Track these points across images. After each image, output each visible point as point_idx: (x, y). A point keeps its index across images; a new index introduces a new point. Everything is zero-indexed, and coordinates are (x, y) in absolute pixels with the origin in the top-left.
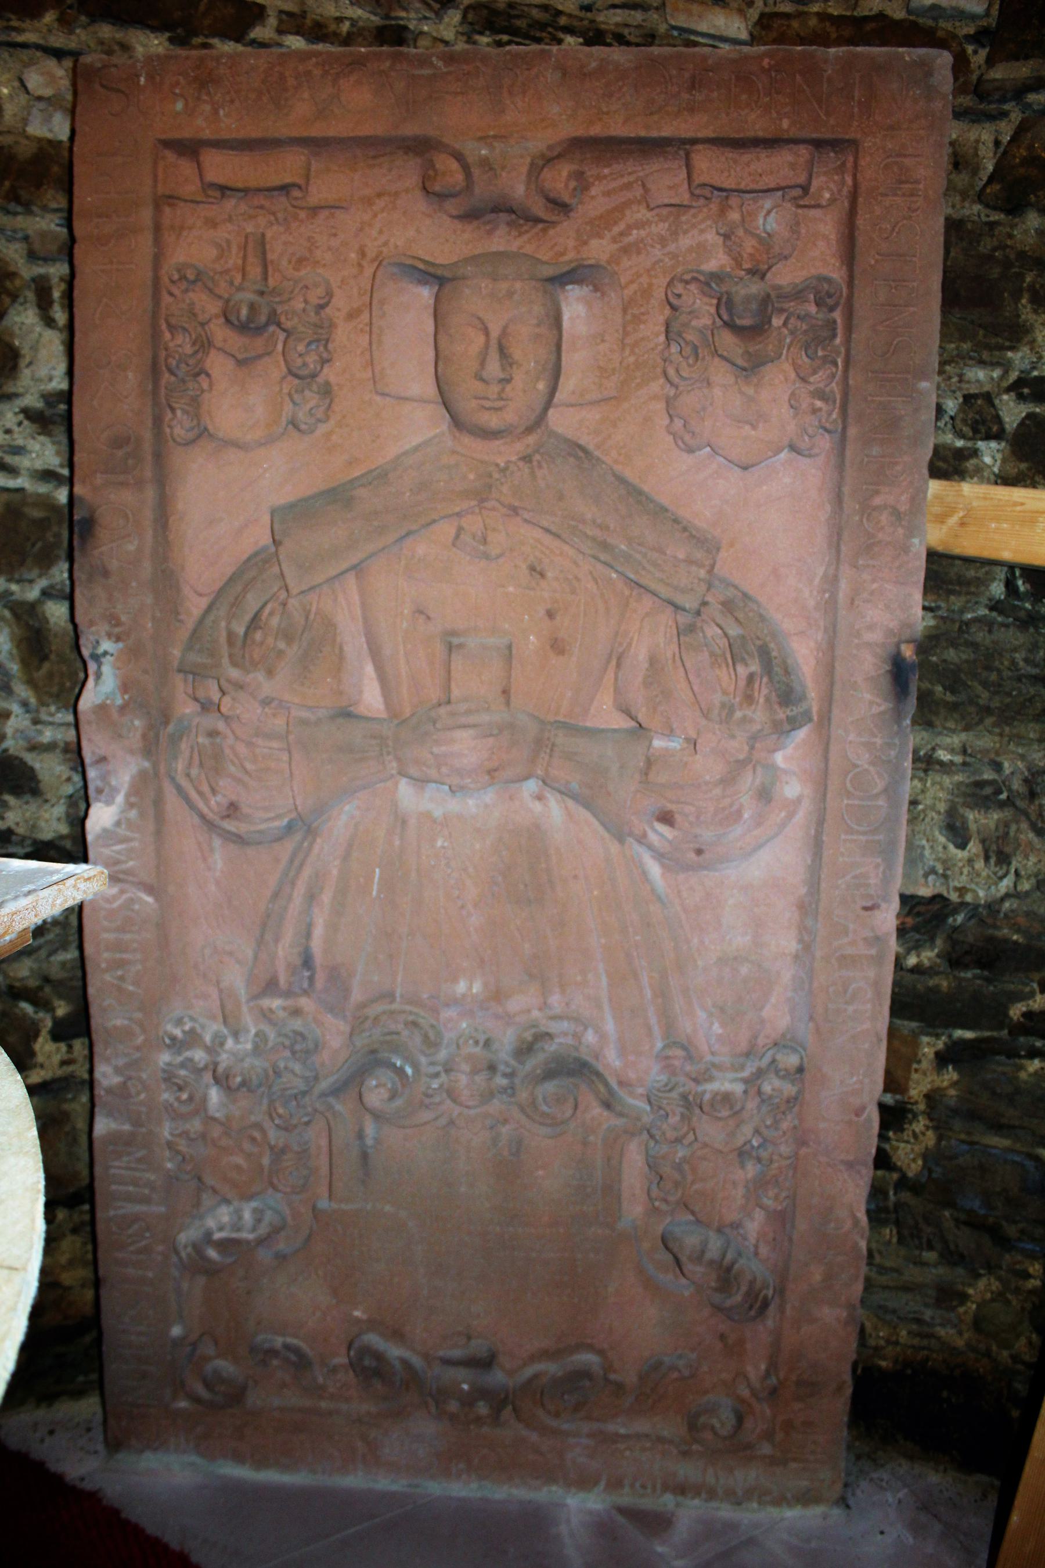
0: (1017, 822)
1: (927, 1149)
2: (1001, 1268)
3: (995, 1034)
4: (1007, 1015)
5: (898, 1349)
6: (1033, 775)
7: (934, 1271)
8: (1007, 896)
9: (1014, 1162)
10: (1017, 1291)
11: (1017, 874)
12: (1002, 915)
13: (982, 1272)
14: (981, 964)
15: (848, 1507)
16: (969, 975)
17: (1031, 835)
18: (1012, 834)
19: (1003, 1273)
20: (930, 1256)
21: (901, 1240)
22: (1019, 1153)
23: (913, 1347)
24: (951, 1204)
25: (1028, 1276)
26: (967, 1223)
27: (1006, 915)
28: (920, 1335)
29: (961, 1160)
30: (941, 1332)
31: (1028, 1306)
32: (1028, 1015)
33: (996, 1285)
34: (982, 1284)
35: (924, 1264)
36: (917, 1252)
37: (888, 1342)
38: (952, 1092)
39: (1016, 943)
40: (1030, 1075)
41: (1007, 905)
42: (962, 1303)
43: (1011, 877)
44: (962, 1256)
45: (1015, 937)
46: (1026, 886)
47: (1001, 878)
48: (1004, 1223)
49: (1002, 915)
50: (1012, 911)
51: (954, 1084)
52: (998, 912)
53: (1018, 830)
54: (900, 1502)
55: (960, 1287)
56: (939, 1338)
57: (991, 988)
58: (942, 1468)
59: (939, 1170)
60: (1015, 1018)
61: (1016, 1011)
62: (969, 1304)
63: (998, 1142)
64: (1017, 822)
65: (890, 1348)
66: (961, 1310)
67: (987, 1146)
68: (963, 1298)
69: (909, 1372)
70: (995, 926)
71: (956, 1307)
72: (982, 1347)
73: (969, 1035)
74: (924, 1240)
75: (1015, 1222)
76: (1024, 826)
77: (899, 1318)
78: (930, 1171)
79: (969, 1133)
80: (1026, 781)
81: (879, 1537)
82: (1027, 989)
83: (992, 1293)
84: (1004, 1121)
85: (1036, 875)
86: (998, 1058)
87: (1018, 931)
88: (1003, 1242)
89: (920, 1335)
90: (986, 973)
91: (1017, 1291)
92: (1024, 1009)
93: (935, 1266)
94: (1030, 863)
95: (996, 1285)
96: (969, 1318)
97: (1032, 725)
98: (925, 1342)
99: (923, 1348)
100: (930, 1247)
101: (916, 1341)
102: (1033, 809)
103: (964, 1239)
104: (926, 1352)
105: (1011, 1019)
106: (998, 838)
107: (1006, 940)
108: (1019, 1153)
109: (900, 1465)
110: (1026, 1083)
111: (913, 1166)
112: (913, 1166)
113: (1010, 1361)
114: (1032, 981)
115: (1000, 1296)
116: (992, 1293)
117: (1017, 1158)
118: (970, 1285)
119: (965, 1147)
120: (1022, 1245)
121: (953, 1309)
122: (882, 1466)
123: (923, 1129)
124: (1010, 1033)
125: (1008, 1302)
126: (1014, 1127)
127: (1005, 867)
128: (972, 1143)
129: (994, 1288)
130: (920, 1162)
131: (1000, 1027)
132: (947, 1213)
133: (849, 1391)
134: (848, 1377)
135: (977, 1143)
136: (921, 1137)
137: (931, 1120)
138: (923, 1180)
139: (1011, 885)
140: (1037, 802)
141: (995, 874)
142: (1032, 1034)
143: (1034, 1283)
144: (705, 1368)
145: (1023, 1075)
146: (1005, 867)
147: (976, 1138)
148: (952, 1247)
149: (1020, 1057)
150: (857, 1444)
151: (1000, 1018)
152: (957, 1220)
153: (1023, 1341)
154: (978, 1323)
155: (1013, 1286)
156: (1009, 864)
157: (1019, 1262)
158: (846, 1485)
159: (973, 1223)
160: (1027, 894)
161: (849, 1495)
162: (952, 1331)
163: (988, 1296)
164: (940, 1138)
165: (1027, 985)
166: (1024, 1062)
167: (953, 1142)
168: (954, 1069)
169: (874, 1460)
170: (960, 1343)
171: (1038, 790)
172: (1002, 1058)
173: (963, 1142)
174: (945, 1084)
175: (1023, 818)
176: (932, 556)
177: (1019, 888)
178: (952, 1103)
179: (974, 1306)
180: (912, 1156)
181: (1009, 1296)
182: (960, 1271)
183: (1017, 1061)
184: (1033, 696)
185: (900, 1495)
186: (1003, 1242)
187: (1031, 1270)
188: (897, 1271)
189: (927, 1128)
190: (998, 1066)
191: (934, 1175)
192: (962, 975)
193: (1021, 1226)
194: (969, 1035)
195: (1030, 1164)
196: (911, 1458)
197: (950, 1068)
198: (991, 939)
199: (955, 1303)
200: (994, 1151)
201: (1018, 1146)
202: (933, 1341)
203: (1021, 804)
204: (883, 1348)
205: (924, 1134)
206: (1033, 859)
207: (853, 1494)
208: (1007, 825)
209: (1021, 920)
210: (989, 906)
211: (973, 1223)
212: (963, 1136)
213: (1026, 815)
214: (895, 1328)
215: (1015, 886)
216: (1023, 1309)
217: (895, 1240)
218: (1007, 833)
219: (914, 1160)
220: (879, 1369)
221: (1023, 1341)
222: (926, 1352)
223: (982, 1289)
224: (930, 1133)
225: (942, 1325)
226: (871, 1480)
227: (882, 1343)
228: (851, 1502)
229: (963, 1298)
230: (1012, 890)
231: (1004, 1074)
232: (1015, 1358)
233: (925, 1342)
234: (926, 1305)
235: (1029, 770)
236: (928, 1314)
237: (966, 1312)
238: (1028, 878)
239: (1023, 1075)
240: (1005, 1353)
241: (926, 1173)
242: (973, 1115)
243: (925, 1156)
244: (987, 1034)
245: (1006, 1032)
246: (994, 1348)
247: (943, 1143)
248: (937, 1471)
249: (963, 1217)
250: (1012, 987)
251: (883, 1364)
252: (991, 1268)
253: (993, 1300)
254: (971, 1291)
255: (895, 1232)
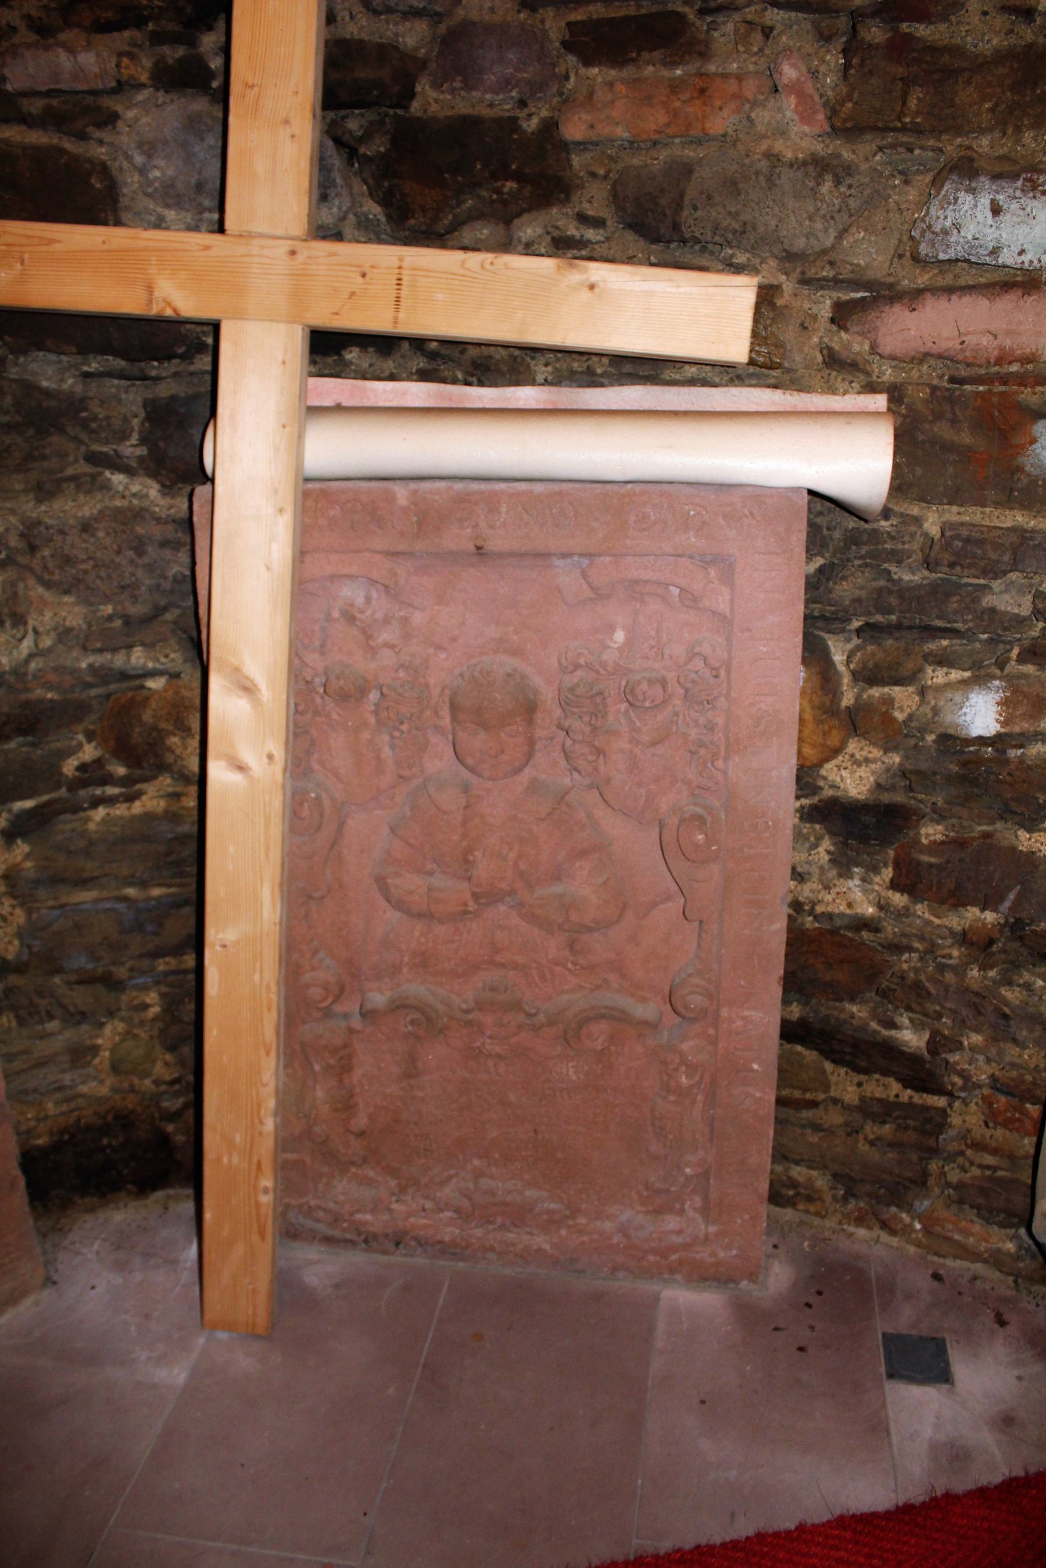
0: (24, 580)
1: (19, 927)
2: (120, 1009)
3: (53, 795)
4: (61, 774)
5: (50, 1122)
6: (28, 528)
7: (61, 1038)
8: (31, 656)
9: (108, 909)
10: (142, 1023)
11: (36, 631)
12: (30, 677)
13: (104, 1020)
14: (22, 731)
15: (55, 1283)
16: (12, 745)
17: (40, 590)
18: (21, 593)
19: (123, 1013)
20: (53, 1025)
21: (21, 1022)
22: (107, 899)
23: (63, 1114)
24: (59, 970)
25: (146, 1007)
26: (80, 982)
27: (35, 676)
28: (67, 1100)
29: (55, 927)
30: (84, 1089)
31: (155, 1032)
32: (82, 767)
33: (121, 1027)
34: (108, 1030)
35: (52, 1034)
36: (40, 1027)
37: (39, 1120)
38: (28, 864)
39: (51, 701)
40: (98, 824)
41: (33, 666)
42: (95, 1055)
43: (31, 635)
44: (83, 1014)
45: (49, 696)
46: (47, 642)
47: (21, 640)
48: (113, 969)
49: (30, 677)
50: (40, 670)
51: (27, 857)
52: (25, 674)
53: (26, 587)
54: (98, 1253)
55: (88, 1042)
56: (82, 1096)
57: (39, 752)
58: (121, 1204)
59: (38, 943)
60: (70, 774)
61: (69, 767)
62: (102, 1053)
63: (86, 896)
64: (24, 580)
65: (42, 1125)
66: (97, 1061)
67: (76, 904)
68: (95, 1049)
69: (66, 1137)
70: (27, 690)
71: (90, 1061)
72: (126, 1085)
73: (29, 804)
74: (43, 1014)
75: (122, 964)
76: (31, 582)
77: (41, 1094)
78: (29, 947)
79: (55, 898)
80: (22, 535)
81: (93, 1292)
82: (74, 743)
83: (120, 1034)
84: (87, 875)
85: (55, 629)
86: (62, 817)
87: (51, 687)
88: (114, 985)
89: (67, 1100)
90: (30, 738)
91: (142, 1023)
92: (76, 763)
93: (60, 1033)
94: (46, 618)
95: (121, 1027)
96: (107, 1066)
97: (14, 476)
98: (73, 1105)
99: (72, 1111)
100: (51, 1017)
101: (64, 1108)
102: (36, 563)
103: (80, 998)
104: (76, 1113)
105: (67, 777)
106: (7, 600)
107: (42, 701)
108: (107, 899)
109: (85, 1222)
110: (96, 832)
111: (11, 948)
112: (11, 948)
113: (153, 1087)
114: (76, 733)
115: (128, 1034)
116: (120, 1034)
117: (108, 905)
118: (98, 1036)
119: (57, 912)
120: (134, 982)
121: (89, 1064)
122: (70, 1231)
123: (9, 909)
124: (69, 790)
125: (136, 1037)
126: (97, 878)
127: (22, 629)
128: (62, 906)
129: (120, 1030)
130: (16, 942)
131: (58, 786)
132: (57, 980)
133: (22, 1183)
134: (17, 1172)
135: (66, 905)
136: (10, 918)
137: (15, 898)
138: (25, 957)
139: (32, 644)
140: (38, 556)
141: (13, 637)
142: (91, 785)
143: (155, 1010)
144: (345, 1225)
145: (92, 826)
146: (22, 629)
147: (64, 900)
148: (72, 1009)
149: (84, 810)
150: (39, 1223)
151: (55, 779)
152: (69, 983)
153: (159, 1065)
154: (116, 1068)
155: (136, 1021)
156: (25, 624)
157: (135, 998)
158: (46, 1263)
159: (86, 980)
160: (50, 650)
161: (52, 1273)
162: (94, 1084)
163: (117, 1038)
164: (29, 912)
165: (72, 739)
166: (90, 813)
167: (44, 911)
168: (24, 842)
169: (60, 1230)
170: (104, 1091)
171: (37, 542)
172: (68, 816)
173: (53, 908)
174: (19, 858)
175: (28, 575)
176: (888, 1339)
177: (41, 646)
178: (32, 874)
179: (107, 1054)
180: (7, 940)
181: (135, 1031)
182: (85, 1027)
183: (82, 814)
184: (10, 446)
185: (96, 1247)
186: (114, 985)
187: (148, 1000)
188: (24, 1052)
189: (13, 907)
190: (66, 826)
191: (35, 950)
192: (6, 747)
193: (128, 965)
194: (29, 804)
195: (121, 906)
196: (92, 1210)
197: (19, 841)
198: (27, 703)
199: (89, 1058)
200: (85, 906)
201: (105, 894)
202: (80, 1100)
203: (22, 560)
204: (35, 1127)
205: (12, 914)
206: (48, 614)
207: (56, 1271)
208: (13, 585)
209: (52, 677)
210: (14, 671)
211: (86, 980)
212: (51, 903)
213: (31, 570)
214: (40, 1104)
215: (36, 644)
216: (151, 1037)
217: (14, 1024)
218: (16, 593)
219: (10, 943)
220: (38, 1148)
221: (159, 1065)
222: (76, 1113)
223: (110, 1033)
224: (18, 911)
225: (84, 1082)
226: (65, 1248)
227: (32, 1123)
228: (55, 1278)
229: (95, 1049)
230: (35, 651)
231: (74, 830)
232: (156, 1082)
233: (73, 1105)
234: (63, 1071)
235: (23, 523)
236: (67, 1079)
237: (101, 1063)
238: (48, 634)
239: (92, 826)
240: (147, 1082)
241: (26, 951)
242: (56, 880)
243: (19, 934)
244: (45, 798)
245: (64, 789)
246: (136, 1081)
247: (34, 916)
248: (118, 1209)
249: (73, 977)
250: (58, 744)
251: (40, 1142)
252: (111, 1014)
253: (122, 1041)
254: (100, 1041)
255: (11, 1016)
